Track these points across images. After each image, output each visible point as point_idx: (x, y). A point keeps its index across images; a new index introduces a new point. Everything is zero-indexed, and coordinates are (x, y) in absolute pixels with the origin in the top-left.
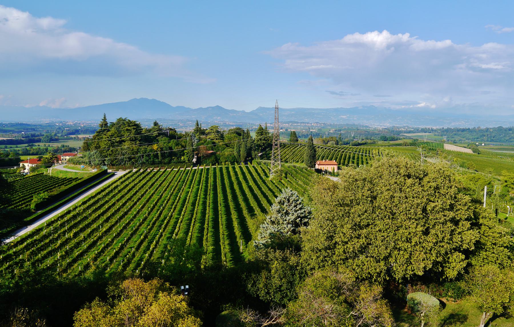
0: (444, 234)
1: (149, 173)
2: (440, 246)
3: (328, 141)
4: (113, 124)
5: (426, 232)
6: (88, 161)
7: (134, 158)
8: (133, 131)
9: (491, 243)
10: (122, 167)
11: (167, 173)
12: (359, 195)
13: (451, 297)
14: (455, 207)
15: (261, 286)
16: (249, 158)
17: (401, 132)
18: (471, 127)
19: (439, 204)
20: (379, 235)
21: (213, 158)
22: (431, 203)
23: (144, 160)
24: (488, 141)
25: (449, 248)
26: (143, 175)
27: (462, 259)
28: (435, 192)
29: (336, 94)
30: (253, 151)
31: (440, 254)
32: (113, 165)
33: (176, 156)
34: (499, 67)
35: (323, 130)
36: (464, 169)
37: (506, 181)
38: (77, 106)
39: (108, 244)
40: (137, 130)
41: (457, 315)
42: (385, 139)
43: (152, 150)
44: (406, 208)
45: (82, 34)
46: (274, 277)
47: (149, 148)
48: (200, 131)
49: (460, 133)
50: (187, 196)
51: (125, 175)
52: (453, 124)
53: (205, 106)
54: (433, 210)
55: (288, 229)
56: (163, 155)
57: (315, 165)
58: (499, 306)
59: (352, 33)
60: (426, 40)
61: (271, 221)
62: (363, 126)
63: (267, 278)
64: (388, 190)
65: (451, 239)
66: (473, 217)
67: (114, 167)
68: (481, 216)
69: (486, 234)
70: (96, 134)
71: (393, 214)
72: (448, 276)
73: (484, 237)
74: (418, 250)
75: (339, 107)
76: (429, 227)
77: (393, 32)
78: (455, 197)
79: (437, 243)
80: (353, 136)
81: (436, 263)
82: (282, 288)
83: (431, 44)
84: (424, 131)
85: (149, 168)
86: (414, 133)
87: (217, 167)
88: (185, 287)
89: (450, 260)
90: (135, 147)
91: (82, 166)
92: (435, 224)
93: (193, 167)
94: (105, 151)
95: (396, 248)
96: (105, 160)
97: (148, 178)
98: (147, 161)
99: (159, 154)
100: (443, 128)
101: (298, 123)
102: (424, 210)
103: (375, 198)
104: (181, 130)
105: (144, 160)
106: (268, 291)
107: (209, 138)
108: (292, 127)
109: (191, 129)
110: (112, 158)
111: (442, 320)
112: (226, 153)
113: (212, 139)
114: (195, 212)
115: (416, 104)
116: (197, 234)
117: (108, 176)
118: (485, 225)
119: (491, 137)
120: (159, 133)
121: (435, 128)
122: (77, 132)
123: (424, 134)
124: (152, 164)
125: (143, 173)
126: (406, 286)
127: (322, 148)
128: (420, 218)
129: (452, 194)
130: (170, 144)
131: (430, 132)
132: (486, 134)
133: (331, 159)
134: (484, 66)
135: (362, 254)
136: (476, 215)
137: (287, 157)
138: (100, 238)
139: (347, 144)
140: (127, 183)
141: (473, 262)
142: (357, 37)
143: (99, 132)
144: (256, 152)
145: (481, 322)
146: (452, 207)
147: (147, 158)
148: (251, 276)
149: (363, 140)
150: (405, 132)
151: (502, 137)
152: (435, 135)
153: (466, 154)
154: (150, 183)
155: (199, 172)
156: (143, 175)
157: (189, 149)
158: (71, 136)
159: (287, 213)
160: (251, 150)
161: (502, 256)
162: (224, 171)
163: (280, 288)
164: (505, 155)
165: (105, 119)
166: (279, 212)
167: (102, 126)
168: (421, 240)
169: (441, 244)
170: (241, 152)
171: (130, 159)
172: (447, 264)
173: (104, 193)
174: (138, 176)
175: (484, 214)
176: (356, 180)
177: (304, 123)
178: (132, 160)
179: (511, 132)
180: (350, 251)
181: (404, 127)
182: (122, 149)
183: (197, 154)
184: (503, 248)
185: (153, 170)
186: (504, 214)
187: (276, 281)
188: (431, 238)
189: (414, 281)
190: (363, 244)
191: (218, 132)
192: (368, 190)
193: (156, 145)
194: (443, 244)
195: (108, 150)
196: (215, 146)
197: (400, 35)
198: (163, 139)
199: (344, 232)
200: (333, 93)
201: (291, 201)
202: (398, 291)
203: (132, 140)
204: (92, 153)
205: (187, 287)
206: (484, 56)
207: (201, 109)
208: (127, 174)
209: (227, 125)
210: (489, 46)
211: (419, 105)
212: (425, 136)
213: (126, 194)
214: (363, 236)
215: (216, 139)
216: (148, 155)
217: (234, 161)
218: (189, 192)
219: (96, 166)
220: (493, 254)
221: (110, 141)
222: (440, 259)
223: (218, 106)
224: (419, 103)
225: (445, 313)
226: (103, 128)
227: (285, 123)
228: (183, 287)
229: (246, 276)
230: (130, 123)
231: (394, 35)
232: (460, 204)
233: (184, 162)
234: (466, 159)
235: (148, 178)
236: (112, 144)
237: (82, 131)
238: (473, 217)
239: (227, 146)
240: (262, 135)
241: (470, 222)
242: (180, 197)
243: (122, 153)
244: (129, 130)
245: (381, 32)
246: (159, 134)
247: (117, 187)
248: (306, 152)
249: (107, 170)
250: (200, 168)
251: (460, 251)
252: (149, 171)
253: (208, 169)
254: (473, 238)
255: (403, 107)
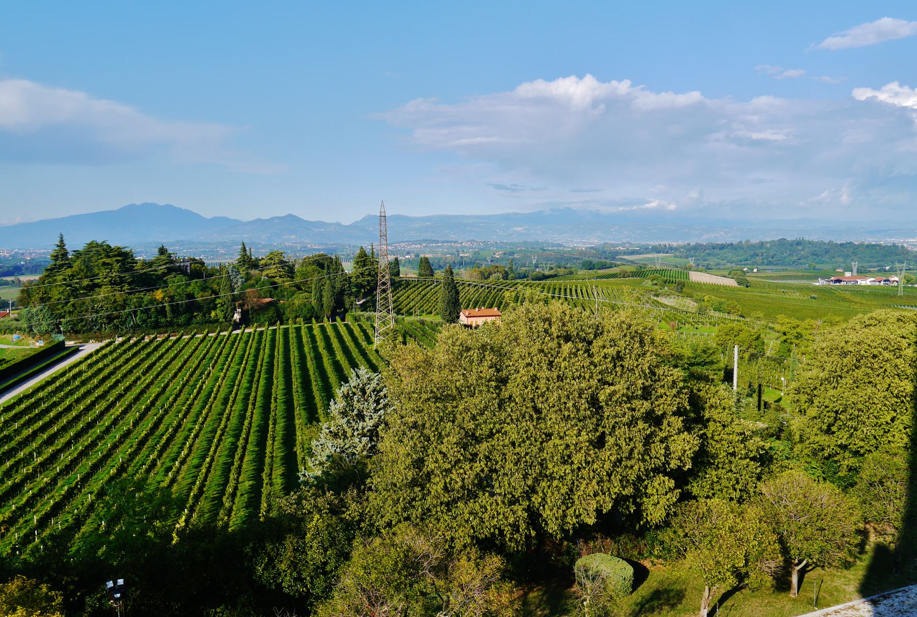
0: (632, 444)
1: (148, 344)
2: (626, 467)
3: (490, 274)
4: (78, 254)
5: (600, 443)
6: (25, 326)
7: (117, 317)
8: (117, 266)
9: (725, 454)
10: (94, 335)
11: (195, 343)
12: (472, 379)
13: (659, 557)
14: (653, 392)
15: (283, 566)
16: (339, 309)
17: (617, 253)
18: (735, 242)
19: (620, 387)
20: (509, 451)
21: (271, 312)
22: (606, 386)
23: (138, 320)
24: (763, 263)
25: (642, 469)
26: (135, 350)
27: (670, 488)
28: (615, 366)
29: (506, 188)
30: (346, 297)
31: (628, 481)
32: (77, 332)
33: (200, 311)
34: (780, 137)
35: (483, 254)
36: (721, 315)
37: (785, 334)
38: (17, 220)
39: (41, 490)
40: (123, 264)
41: (667, 591)
42: (590, 266)
43: (152, 301)
44: (560, 400)
45: (26, 84)
46: (311, 547)
47: (147, 298)
48: (249, 262)
49: (717, 251)
50: (214, 386)
51: (97, 352)
52: (705, 237)
53: (266, 216)
54: (611, 400)
55: (361, 445)
56: (175, 310)
57: (458, 317)
58: (729, 573)
59: (531, 79)
60: (658, 92)
61: (331, 432)
62: (553, 245)
63: (296, 550)
64: (529, 365)
65: (647, 452)
66: (688, 408)
67: (79, 336)
68: (708, 405)
69: (716, 438)
70: (45, 274)
71: (538, 411)
72: (649, 519)
73: (714, 443)
74: (585, 476)
75: (511, 211)
76: (603, 433)
77: (603, 78)
78: (653, 373)
79: (620, 461)
80: (534, 262)
81: (620, 500)
82: (328, 568)
83: (667, 99)
84: (656, 249)
85: (148, 334)
86: (640, 254)
87: (280, 328)
88: (115, 583)
89: (649, 491)
90: (119, 296)
91: (15, 336)
92: (614, 427)
93: (234, 329)
94: (60, 307)
95: (546, 476)
96: (60, 323)
97: (143, 355)
98: (144, 321)
99: (168, 309)
100: (689, 244)
101: (438, 242)
102: (594, 402)
103: (504, 381)
104: (211, 262)
105: (138, 320)
106: (299, 574)
107: (267, 275)
108: (427, 250)
109: (232, 259)
110: (74, 318)
111: (637, 605)
112: (296, 302)
113: (272, 277)
114: (225, 416)
115: (641, 203)
116: (224, 458)
117: (64, 353)
118: (714, 421)
119: (768, 256)
120: (167, 268)
121: (675, 244)
122: (17, 270)
123: (655, 255)
124: (154, 328)
125: (135, 344)
126: (575, 544)
127: (475, 286)
128: (585, 417)
129: (646, 367)
130: (190, 289)
131: (667, 252)
132: (759, 252)
133: (491, 307)
134: (756, 136)
135: (484, 491)
136: (696, 403)
137: (411, 304)
138: (30, 477)
139: (524, 277)
140: (100, 365)
141: (695, 491)
142: (540, 87)
143: (52, 270)
144: (352, 298)
145: (703, 605)
146: (646, 393)
147: (145, 317)
148: (264, 548)
149: (552, 269)
150: (625, 253)
151: (786, 257)
152: (676, 257)
153: (725, 287)
154: (146, 364)
155: (245, 339)
156: (135, 350)
157: (225, 295)
158: (4, 279)
159: (361, 416)
160: (343, 295)
161: (745, 477)
162: (292, 335)
163: (323, 569)
164: (790, 288)
165: (62, 245)
166: (344, 414)
167: (56, 258)
168: (589, 459)
169: (629, 463)
170: (324, 299)
171: (110, 319)
172: (645, 499)
173: (50, 388)
174: (125, 352)
175: (713, 401)
176: (468, 349)
177: (448, 242)
178: (114, 321)
179: (800, 247)
180: (457, 487)
181: (623, 245)
182: (93, 301)
183: (241, 306)
184: (748, 460)
185: (156, 338)
186: (778, 392)
187: (314, 555)
188: (608, 454)
189: (583, 532)
190: (482, 471)
191: (281, 262)
192: (491, 367)
193: (160, 291)
194: (632, 462)
195: (67, 303)
196: (276, 288)
197: (614, 83)
198: (176, 280)
199: (444, 450)
200: (499, 187)
201: (368, 392)
202: (561, 554)
203: (115, 283)
204: (35, 310)
205: (121, 582)
206: (755, 118)
207: (259, 221)
208: (102, 348)
209: (299, 248)
210: (763, 101)
211: (647, 205)
212: (658, 258)
213: (97, 387)
214: (481, 456)
215: (280, 277)
216: (147, 311)
217: (312, 315)
218: (217, 379)
219: (42, 335)
220: (730, 474)
221: (70, 285)
222: (629, 491)
223: (290, 216)
224: (649, 202)
225: (645, 590)
226: (59, 262)
227: (415, 242)
228: (110, 584)
229: (254, 550)
230: (108, 251)
231: (604, 83)
232: (664, 386)
233: (217, 321)
234: (725, 298)
235: (143, 355)
236: (74, 293)
237: (27, 268)
238: (688, 408)
239: (299, 288)
240: (364, 265)
241: (681, 418)
242: (201, 388)
243: (93, 308)
244: (108, 264)
245: (581, 77)
246: (170, 271)
247: (80, 373)
248: (441, 294)
249: (63, 342)
250: (247, 331)
251: (666, 474)
252: (147, 340)
253: (261, 333)
254: (687, 448)
255: (621, 208)
